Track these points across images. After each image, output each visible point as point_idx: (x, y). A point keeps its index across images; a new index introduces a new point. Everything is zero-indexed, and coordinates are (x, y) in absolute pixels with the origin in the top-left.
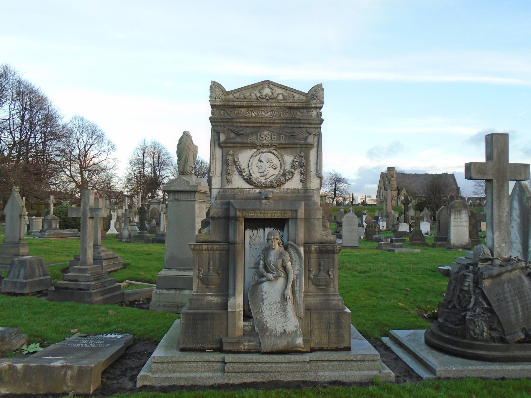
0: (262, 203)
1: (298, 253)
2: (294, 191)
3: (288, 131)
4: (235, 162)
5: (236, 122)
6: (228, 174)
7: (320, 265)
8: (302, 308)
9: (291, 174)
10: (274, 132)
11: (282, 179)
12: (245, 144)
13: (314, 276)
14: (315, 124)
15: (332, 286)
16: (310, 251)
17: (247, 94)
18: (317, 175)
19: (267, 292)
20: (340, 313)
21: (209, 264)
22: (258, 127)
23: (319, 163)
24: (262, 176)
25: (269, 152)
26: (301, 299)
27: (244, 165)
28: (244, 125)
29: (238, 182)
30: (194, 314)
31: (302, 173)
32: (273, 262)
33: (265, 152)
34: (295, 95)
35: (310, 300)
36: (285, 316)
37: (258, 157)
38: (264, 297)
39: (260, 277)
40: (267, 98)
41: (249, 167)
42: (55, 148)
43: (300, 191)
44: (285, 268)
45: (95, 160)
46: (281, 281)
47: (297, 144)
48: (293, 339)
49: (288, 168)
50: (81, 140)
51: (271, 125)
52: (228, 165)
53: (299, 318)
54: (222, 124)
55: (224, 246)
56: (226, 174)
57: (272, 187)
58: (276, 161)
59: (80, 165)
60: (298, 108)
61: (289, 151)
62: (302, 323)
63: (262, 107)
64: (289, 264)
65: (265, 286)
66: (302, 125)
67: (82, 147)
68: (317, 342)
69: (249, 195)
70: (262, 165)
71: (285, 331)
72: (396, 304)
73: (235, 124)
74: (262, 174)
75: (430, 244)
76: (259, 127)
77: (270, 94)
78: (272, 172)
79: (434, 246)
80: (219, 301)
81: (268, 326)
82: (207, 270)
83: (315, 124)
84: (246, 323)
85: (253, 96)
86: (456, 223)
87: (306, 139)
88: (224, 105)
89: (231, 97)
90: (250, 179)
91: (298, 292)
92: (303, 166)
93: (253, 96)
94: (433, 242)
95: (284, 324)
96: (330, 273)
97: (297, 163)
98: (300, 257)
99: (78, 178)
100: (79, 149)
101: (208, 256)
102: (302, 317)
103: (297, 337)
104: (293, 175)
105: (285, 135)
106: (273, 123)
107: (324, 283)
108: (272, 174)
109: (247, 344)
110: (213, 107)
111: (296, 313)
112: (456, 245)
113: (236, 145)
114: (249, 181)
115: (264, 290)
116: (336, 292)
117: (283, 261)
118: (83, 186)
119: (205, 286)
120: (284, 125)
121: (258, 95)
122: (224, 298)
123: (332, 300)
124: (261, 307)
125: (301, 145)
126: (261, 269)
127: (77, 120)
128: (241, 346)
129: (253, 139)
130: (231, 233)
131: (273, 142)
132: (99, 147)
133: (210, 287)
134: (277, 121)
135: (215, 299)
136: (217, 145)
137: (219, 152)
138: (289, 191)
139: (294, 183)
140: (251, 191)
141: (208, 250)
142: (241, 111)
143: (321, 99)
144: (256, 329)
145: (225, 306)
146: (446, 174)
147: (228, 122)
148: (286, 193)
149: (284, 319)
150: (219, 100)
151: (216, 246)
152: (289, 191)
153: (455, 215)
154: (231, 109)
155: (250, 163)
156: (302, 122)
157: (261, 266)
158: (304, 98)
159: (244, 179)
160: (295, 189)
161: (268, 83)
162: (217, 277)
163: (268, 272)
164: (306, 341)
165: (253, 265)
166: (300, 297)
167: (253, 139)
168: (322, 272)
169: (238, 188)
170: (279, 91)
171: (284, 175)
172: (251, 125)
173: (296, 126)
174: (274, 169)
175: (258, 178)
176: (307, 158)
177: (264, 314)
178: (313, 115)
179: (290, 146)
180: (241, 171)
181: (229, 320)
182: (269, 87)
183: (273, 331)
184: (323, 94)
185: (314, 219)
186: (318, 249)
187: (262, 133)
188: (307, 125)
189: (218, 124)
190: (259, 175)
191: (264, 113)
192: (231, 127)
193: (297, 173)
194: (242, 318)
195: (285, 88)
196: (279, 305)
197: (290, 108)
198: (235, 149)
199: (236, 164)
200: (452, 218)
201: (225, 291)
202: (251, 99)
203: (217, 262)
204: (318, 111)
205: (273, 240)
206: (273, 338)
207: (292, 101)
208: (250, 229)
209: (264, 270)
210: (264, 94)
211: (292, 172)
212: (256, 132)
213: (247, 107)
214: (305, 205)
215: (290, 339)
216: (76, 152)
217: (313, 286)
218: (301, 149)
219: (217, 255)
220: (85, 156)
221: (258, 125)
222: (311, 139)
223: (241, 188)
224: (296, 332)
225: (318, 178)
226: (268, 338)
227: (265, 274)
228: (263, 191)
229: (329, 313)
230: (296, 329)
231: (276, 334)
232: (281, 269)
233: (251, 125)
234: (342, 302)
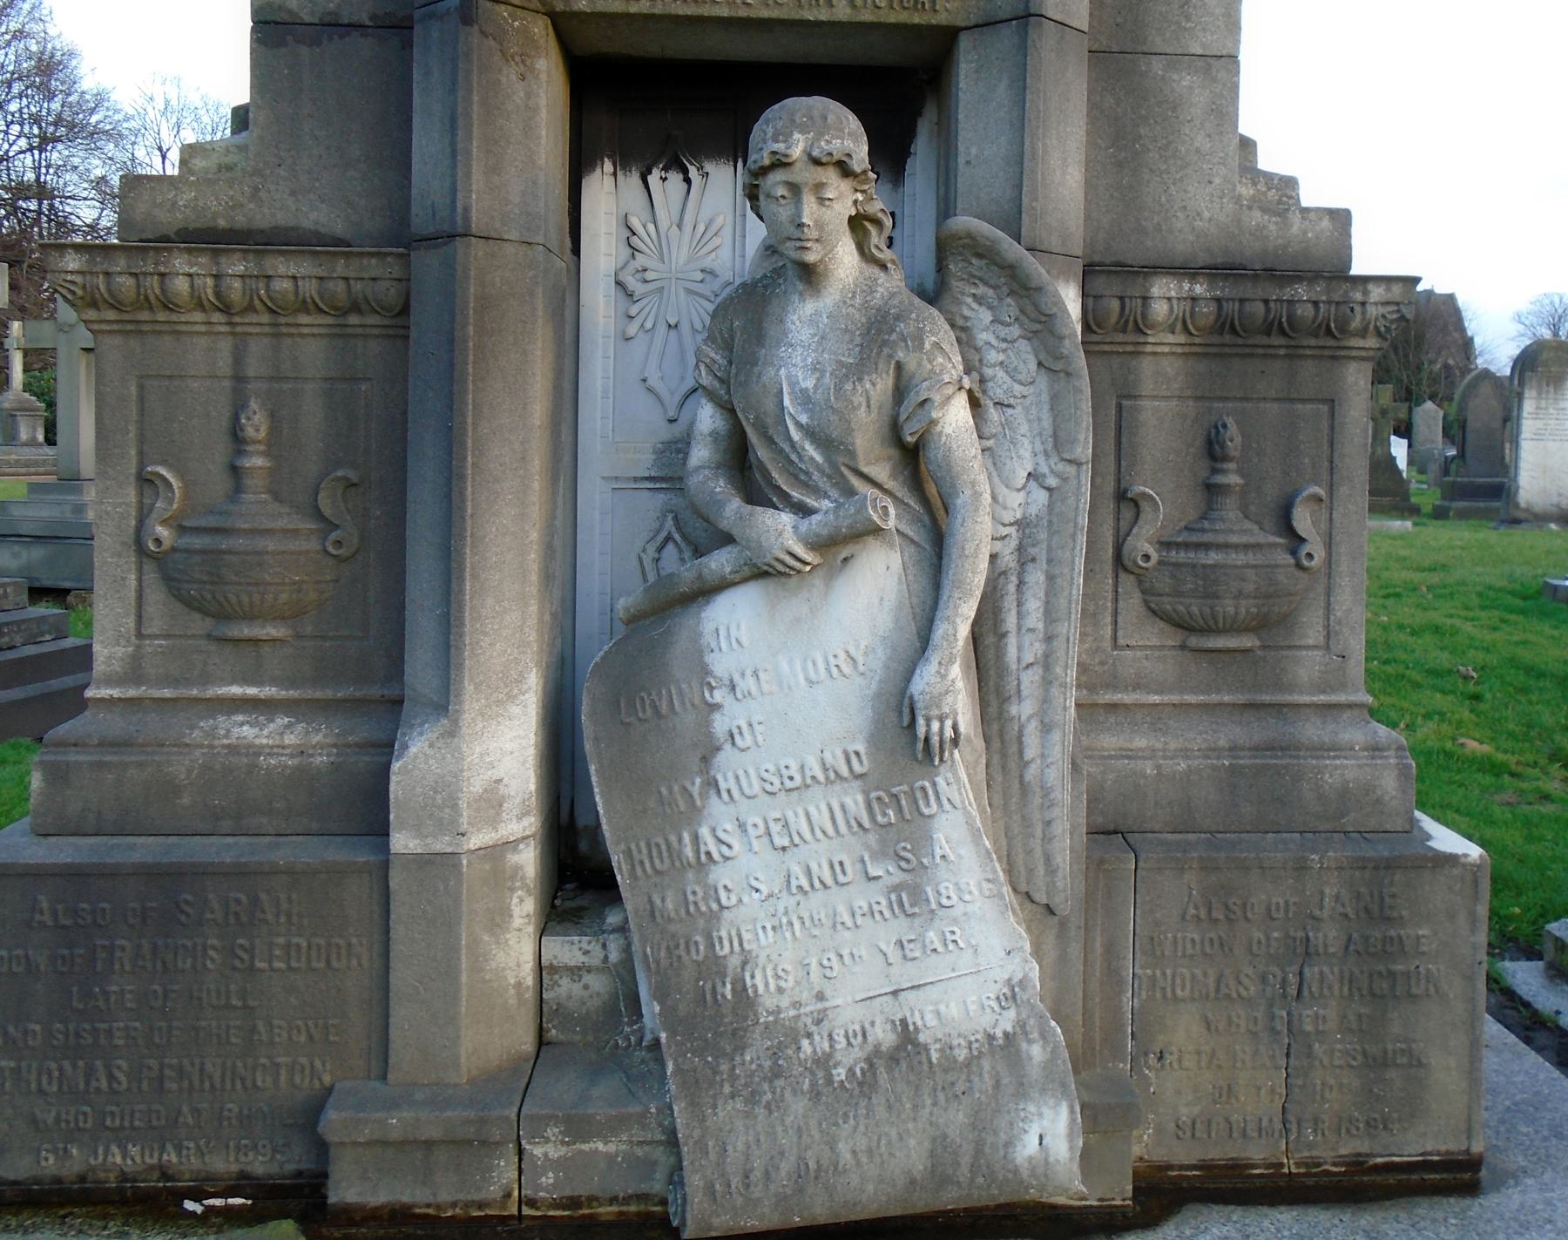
1: (1040, 323)
7: (1214, 451)
8: (1061, 827)
13: (1165, 545)
15: (1314, 635)
16: (1136, 324)
19: (749, 683)
20: (1399, 866)
21: (237, 438)
26: (1060, 747)
30: (74, 875)
32: (805, 399)
35: (1130, 754)
36: (912, 897)
38: (720, 724)
39: (692, 558)
44: (913, 455)
46: (876, 582)
48: (980, 1124)
53: (1038, 910)
55: (375, 276)
62: (1063, 958)
64: (955, 418)
65: (736, 627)
68: (1185, 1113)
71: (907, 1034)
72: (1449, 745)
79: (1439, 514)
80: (320, 760)
81: (758, 981)
82: (219, 484)
84: (566, 949)
86: (1539, 424)
91: (1030, 680)
95: (904, 975)
96: (1303, 520)
98: (1052, 365)
101: (224, 364)
102: (1058, 902)
103: (1022, 1091)
107: (1247, 608)
109: (555, 1151)
111: (1010, 871)
112: (1537, 509)
115: (722, 664)
116: (1343, 686)
117: (900, 392)
119: (200, 624)
122: (364, 730)
123: (1321, 749)
124: (694, 813)
126: (694, 481)
128: (505, 1171)
130: (425, 143)
133: (246, 631)
135: (274, 738)
141: (226, 308)
144: (651, 1009)
145: (364, 806)
149: (899, 927)
151: (289, 273)
153: (1539, 397)
157: (700, 454)
162: (314, 545)
163: (756, 490)
164: (1101, 1119)
165: (644, 462)
166: (1046, 728)
168: (1230, 511)
177: (721, 876)
181: (398, 931)
183: (794, 1035)
185: (1179, 58)
186: (1207, 310)
194: (524, 908)
196: (854, 801)
197: (1529, 670)
200: (1528, 406)
201: (382, 673)
203: (312, 414)
205: (804, 174)
206: (798, 1106)
208: (624, 161)
209: (721, 486)
215: (956, 1119)
217: (1154, 635)
219: (312, 352)
224: (1008, 1047)
226: (753, 1098)
227: (733, 508)
229: (1301, 867)
230: (1007, 1021)
231: (824, 1062)
232: (881, 472)
234: (1403, 771)
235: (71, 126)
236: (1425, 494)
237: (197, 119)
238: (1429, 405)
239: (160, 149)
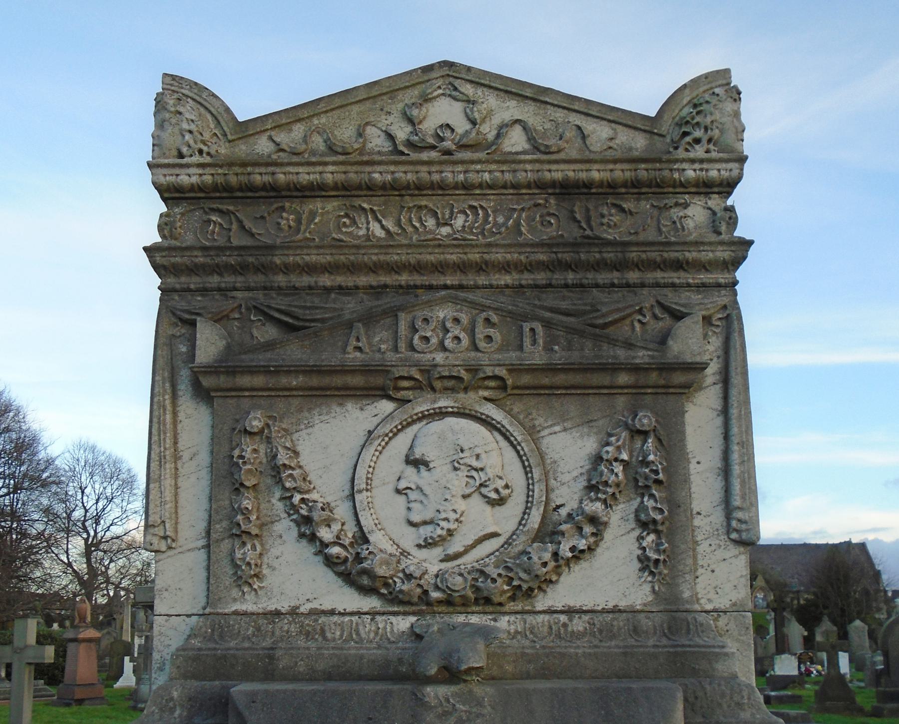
0: (420, 702)
2: (609, 621)
3: (564, 305)
4: (276, 471)
5: (287, 269)
6: (241, 535)
9: (588, 529)
10: (483, 308)
11: (542, 554)
12: (332, 371)
14: (704, 267)
17: (345, 134)
18: (729, 530)
22: (399, 286)
23: (736, 469)
24: (428, 544)
25: (460, 414)
27: (327, 487)
28: (326, 280)
29: (295, 580)
31: (645, 525)
33: (441, 414)
34: (589, 126)
37: (401, 443)
40: (448, 144)
41: (352, 497)
42: (34, 504)
43: (645, 622)
45: (116, 530)
47: (615, 368)
49: (568, 495)
50: (87, 491)
51: (470, 279)
52: (239, 488)
54: (214, 280)
56: (231, 534)
57: (485, 601)
58: (499, 461)
59: (86, 540)
60: (611, 188)
61: (572, 407)
63: (419, 188)
66: (633, 276)
67: (90, 503)
69: (352, 649)
70: (426, 482)
73: (281, 279)
74: (426, 531)
75: (868, 707)
76: (410, 288)
77: (461, 126)
78: (480, 518)
79: (877, 713)
83: (704, 267)
85: (376, 141)
87: (663, 340)
88: (227, 188)
89: (263, 146)
90: (358, 559)
92: (651, 485)
93: (376, 141)
94: (875, 704)
97: (618, 468)
99: (81, 566)
100: (85, 508)
104: (598, 535)
105: (548, 324)
106: (482, 267)
108: (484, 528)
110: (169, 194)
113: (284, 381)
114: (352, 568)
118: (89, 582)
120: (541, 277)
121: (402, 132)
125: (636, 369)
127: (82, 452)
129: (375, 345)
131: (484, 359)
132: (125, 504)
134: (498, 256)
136: (184, 386)
137: (196, 424)
138: (578, 624)
139: (608, 579)
140: (367, 627)
142: (313, 214)
143: (729, 138)
146: (848, 544)
147: (242, 269)
148: (562, 634)
150: (196, 159)
152: (578, 624)
154: (263, 209)
155: (361, 473)
156: (633, 255)
158: (639, 142)
159: (330, 562)
160: (616, 610)
161: (449, 76)
167: (375, 345)
169: (294, 612)
170: (510, 110)
171: (548, 533)
172: (363, 280)
173: (603, 277)
174: (493, 503)
175: (405, 553)
176: (671, 441)
178: (690, 224)
179: (578, 379)
180: (308, 520)
182: (454, 94)
184: (737, 114)
187: (420, 314)
188: (659, 275)
189: (194, 282)
190: (409, 538)
191: (431, 223)
192: (260, 295)
193: (619, 520)
195: (539, 96)
197: (566, 190)
198: (281, 404)
199: (280, 482)
202: (362, 151)
204: (714, 202)
207: (574, 154)
210: (429, 125)
211: (593, 520)
212: (393, 313)
213: (345, 190)
214: (690, 706)
216: (78, 514)
218: (637, 390)
220: (97, 523)
221: (404, 278)
222: (692, 342)
223: (314, 612)
225: (734, 550)
228: (434, 623)
233: (363, 280)
235: (32, 479)
236: (866, 699)
237: (103, 470)
238: (858, 623)
239: (81, 488)
